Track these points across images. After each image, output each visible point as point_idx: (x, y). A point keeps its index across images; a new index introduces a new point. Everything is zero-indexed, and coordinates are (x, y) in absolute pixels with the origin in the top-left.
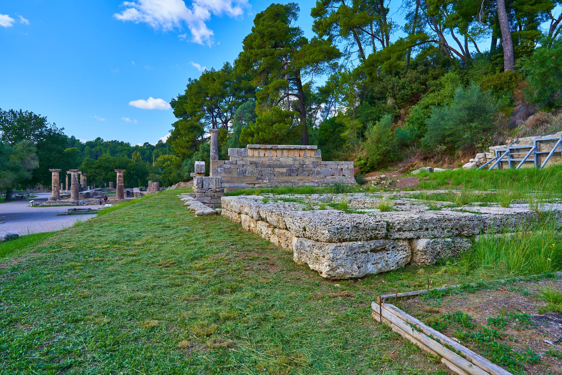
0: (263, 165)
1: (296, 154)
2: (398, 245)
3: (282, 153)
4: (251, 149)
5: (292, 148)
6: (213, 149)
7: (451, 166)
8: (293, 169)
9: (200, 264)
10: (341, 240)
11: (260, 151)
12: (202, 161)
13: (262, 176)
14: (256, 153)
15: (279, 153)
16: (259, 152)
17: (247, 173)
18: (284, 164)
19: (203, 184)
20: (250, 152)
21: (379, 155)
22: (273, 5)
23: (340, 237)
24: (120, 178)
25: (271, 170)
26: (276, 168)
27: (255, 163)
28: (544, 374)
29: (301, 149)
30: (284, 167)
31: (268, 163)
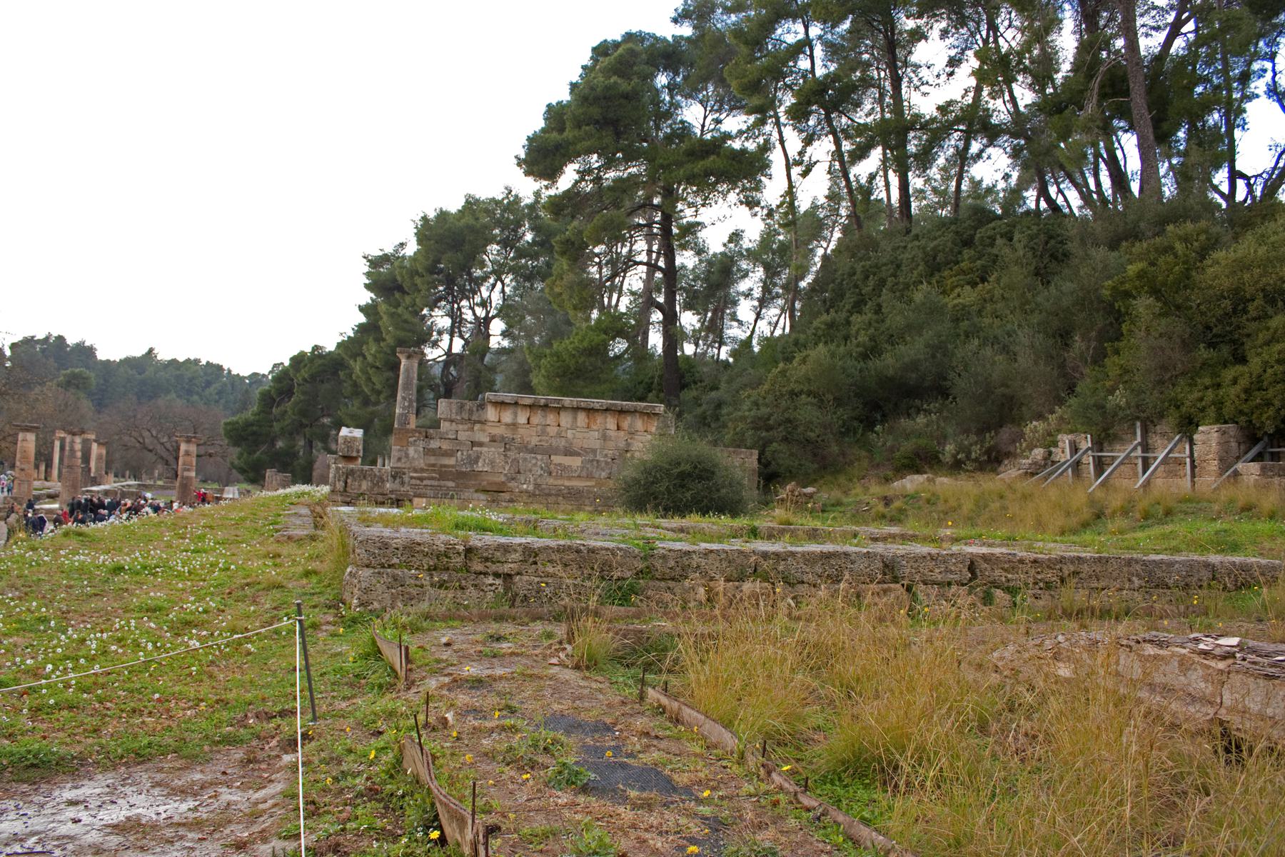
0: (525, 448)
1: (611, 422)
3: (575, 418)
5: (597, 406)
6: (404, 398)
8: (598, 461)
12: (357, 427)
13: (519, 472)
14: (507, 417)
15: (565, 419)
17: (480, 464)
18: (577, 445)
20: (491, 414)
21: (99, 499)
22: (601, 51)
24: (188, 459)
25: (542, 460)
27: (503, 438)
29: (622, 412)
30: (578, 454)
31: (534, 441)
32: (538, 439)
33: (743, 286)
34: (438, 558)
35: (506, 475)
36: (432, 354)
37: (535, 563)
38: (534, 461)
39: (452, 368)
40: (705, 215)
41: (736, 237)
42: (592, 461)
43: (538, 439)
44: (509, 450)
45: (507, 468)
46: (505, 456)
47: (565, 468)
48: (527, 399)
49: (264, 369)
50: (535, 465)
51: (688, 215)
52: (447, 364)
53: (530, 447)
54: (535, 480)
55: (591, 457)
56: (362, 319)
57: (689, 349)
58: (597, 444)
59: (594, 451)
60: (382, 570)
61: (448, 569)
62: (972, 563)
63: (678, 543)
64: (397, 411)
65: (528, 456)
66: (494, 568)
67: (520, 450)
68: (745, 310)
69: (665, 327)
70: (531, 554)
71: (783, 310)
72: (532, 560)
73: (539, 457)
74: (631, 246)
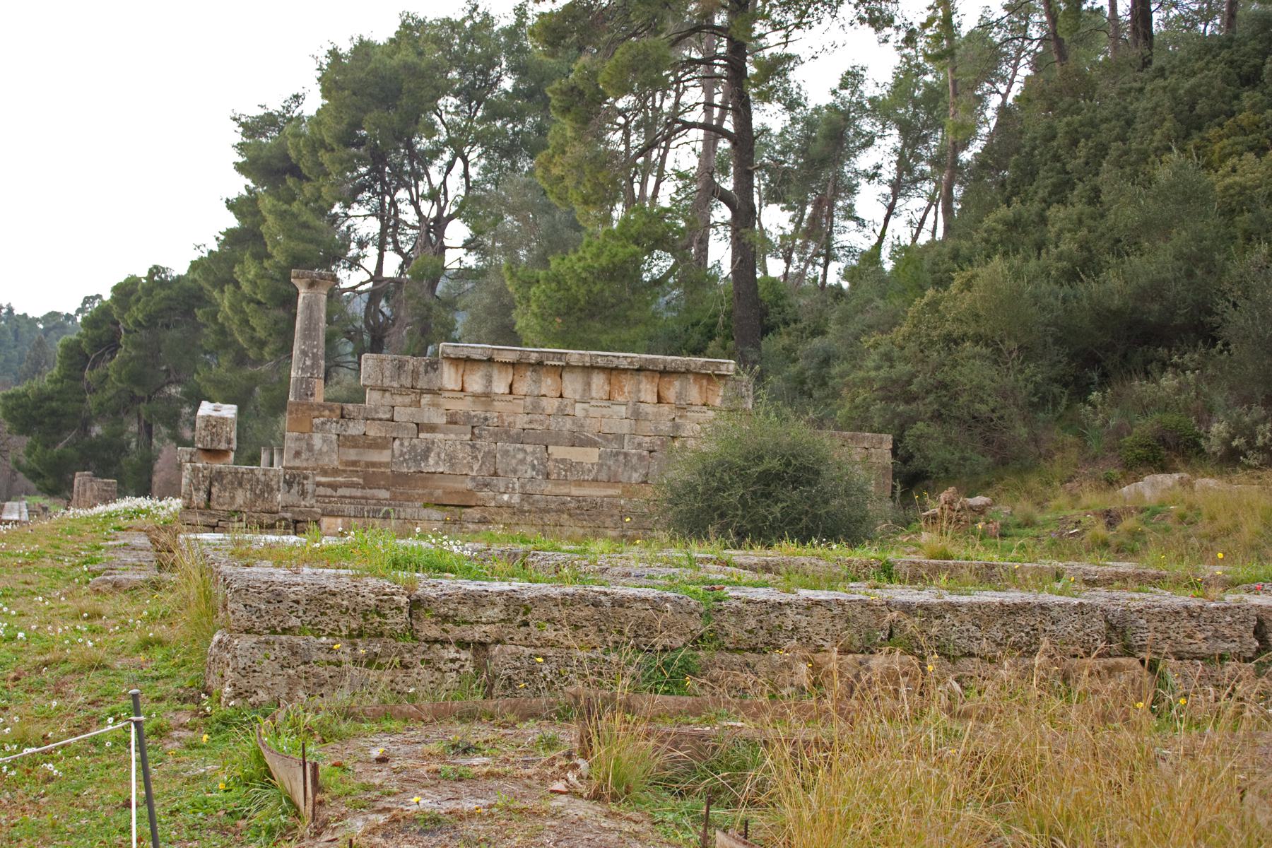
0: (504, 433)
2: (442, 658)
3: (588, 384)
4: (456, 361)
5: (624, 364)
6: (304, 353)
7: (896, 422)
8: (626, 455)
9: (1144, 801)
10: (279, 629)
11: (495, 372)
13: (496, 474)
15: (572, 385)
16: (489, 380)
17: (431, 461)
19: (209, 494)
20: (449, 377)
23: (274, 622)
26: (556, 444)
27: (468, 417)
28: (19, 846)
29: (665, 373)
30: (593, 444)
31: (521, 422)
32: (526, 418)
33: (864, 161)
34: (365, 617)
35: (473, 478)
36: (349, 278)
37: (526, 624)
38: (520, 456)
39: (383, 303)
40: (802, 42)
41: (852, 79)
42: (617, 454)
43: (526, 418)
44: (480, 437)
45: (476, 467)
46: (473, 447)
47: (570, 466)
48: (509, 353)
49: (69, 305)
50: (523, 461)
51: (772, 43)
52: (374, 296)
53: (513, 432)
54: (522, 486)
55: (614, 447)
56: (232, 222)
57: (775, 267)
58: (625, 427)
59: (619, 438)
60: (272, 638)
61: (382, 634)
62: (1261, 622)
63: (762, 590)
64: (293, 374)
65: (511, 447)
66: (456, 632)
67: (496, 437)
68: (869, 200)
69: (735, 231)
70: (518, 609)
71: (932, 201)
72: (519, 618)
73: (529, 448)
74: (678, 96)
